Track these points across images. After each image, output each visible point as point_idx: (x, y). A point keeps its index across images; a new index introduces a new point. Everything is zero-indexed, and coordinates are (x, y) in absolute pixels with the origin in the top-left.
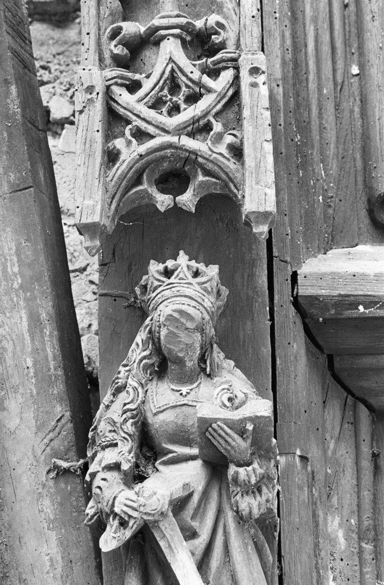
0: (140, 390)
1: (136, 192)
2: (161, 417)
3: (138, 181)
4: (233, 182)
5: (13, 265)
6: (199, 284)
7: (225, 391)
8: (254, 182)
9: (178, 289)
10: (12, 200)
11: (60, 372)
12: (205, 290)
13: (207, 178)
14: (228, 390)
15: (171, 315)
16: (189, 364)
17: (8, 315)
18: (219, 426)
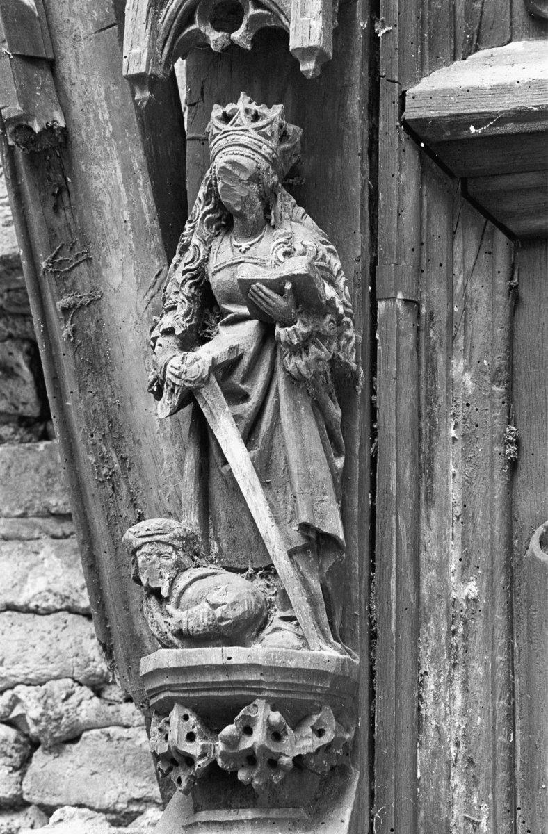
0: (202, 248)
1: (189, 32)
2: (219, 276)
3: (191, 21)
4: (284, 14)
5: (103, 112)
6: (256, 129)
7: (281, 245)
8: (299, 14)
9: (232, 137)
10: (97, 40)
11: (156, 225)
12: (264, 135)
13: (259, 11)
14: (285, 243)
15: (223, 168)
16: (251, 217)
17: (103, 166)
18: (258, 287)
